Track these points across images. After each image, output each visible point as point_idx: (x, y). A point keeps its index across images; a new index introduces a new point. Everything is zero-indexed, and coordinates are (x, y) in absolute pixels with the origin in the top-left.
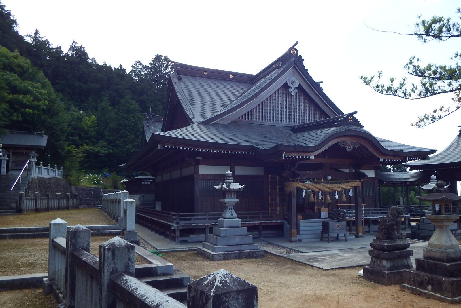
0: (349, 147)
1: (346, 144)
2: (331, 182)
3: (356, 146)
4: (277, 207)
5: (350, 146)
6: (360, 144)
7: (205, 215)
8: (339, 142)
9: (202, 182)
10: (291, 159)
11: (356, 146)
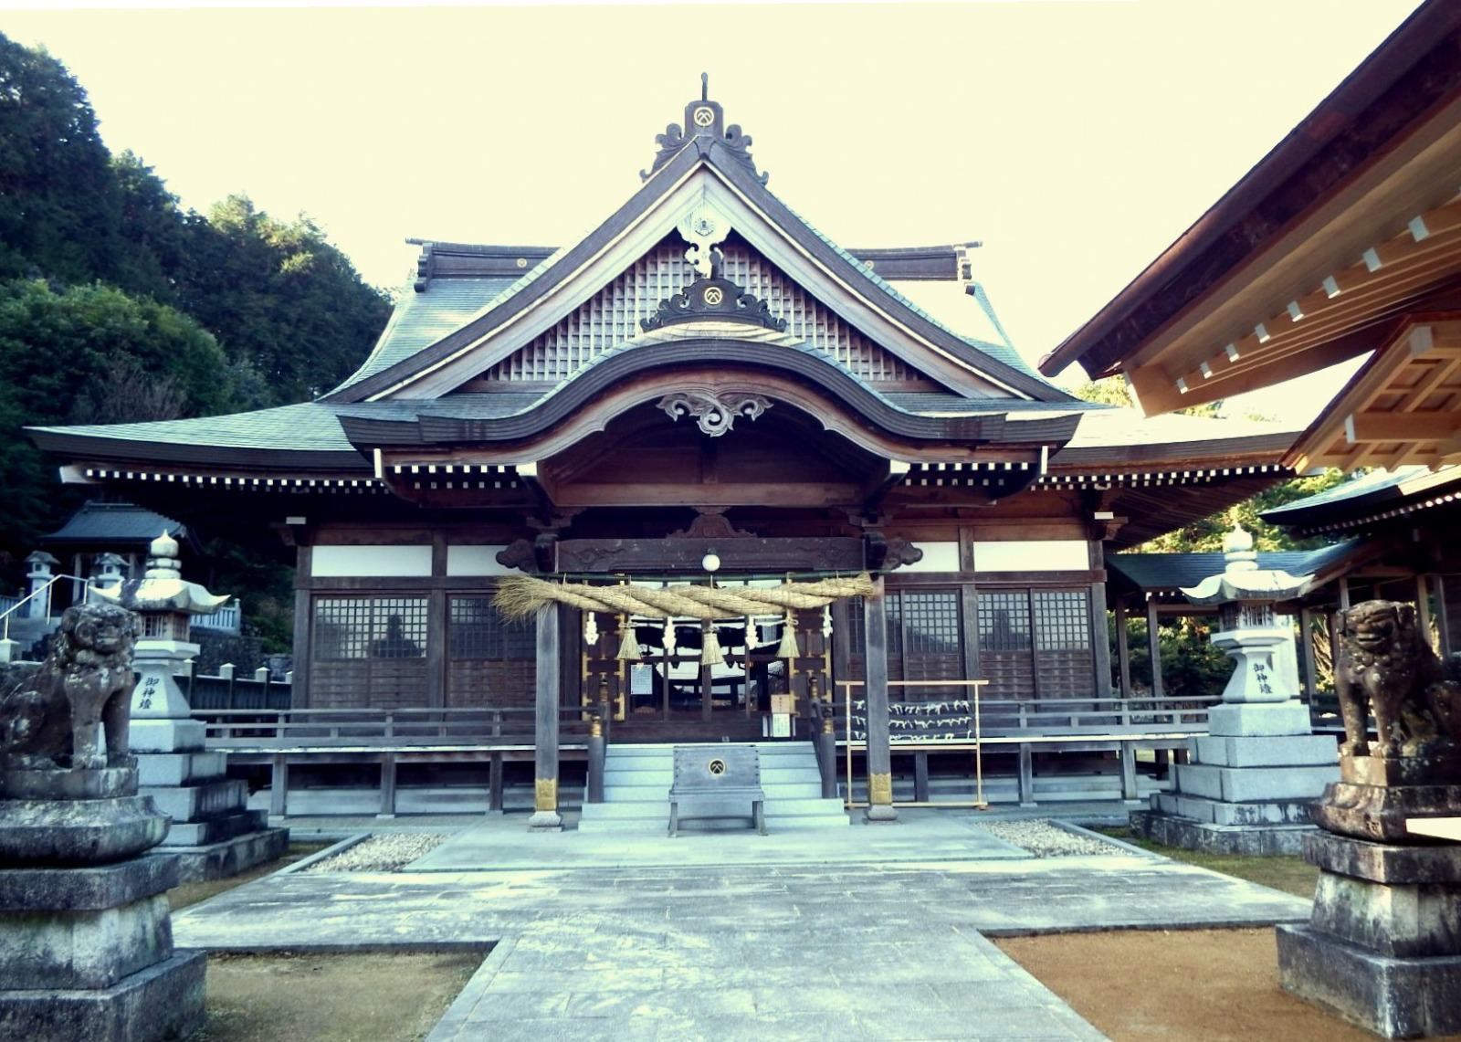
0: (715, 418)
1: (695, 402)
3: (748, 411)
4: (618, 696)
5: (716, 411)
6: (770, 400)
8: (658, 400)
9: (907, 607)
10: (374, 491)
11: (748, 411)
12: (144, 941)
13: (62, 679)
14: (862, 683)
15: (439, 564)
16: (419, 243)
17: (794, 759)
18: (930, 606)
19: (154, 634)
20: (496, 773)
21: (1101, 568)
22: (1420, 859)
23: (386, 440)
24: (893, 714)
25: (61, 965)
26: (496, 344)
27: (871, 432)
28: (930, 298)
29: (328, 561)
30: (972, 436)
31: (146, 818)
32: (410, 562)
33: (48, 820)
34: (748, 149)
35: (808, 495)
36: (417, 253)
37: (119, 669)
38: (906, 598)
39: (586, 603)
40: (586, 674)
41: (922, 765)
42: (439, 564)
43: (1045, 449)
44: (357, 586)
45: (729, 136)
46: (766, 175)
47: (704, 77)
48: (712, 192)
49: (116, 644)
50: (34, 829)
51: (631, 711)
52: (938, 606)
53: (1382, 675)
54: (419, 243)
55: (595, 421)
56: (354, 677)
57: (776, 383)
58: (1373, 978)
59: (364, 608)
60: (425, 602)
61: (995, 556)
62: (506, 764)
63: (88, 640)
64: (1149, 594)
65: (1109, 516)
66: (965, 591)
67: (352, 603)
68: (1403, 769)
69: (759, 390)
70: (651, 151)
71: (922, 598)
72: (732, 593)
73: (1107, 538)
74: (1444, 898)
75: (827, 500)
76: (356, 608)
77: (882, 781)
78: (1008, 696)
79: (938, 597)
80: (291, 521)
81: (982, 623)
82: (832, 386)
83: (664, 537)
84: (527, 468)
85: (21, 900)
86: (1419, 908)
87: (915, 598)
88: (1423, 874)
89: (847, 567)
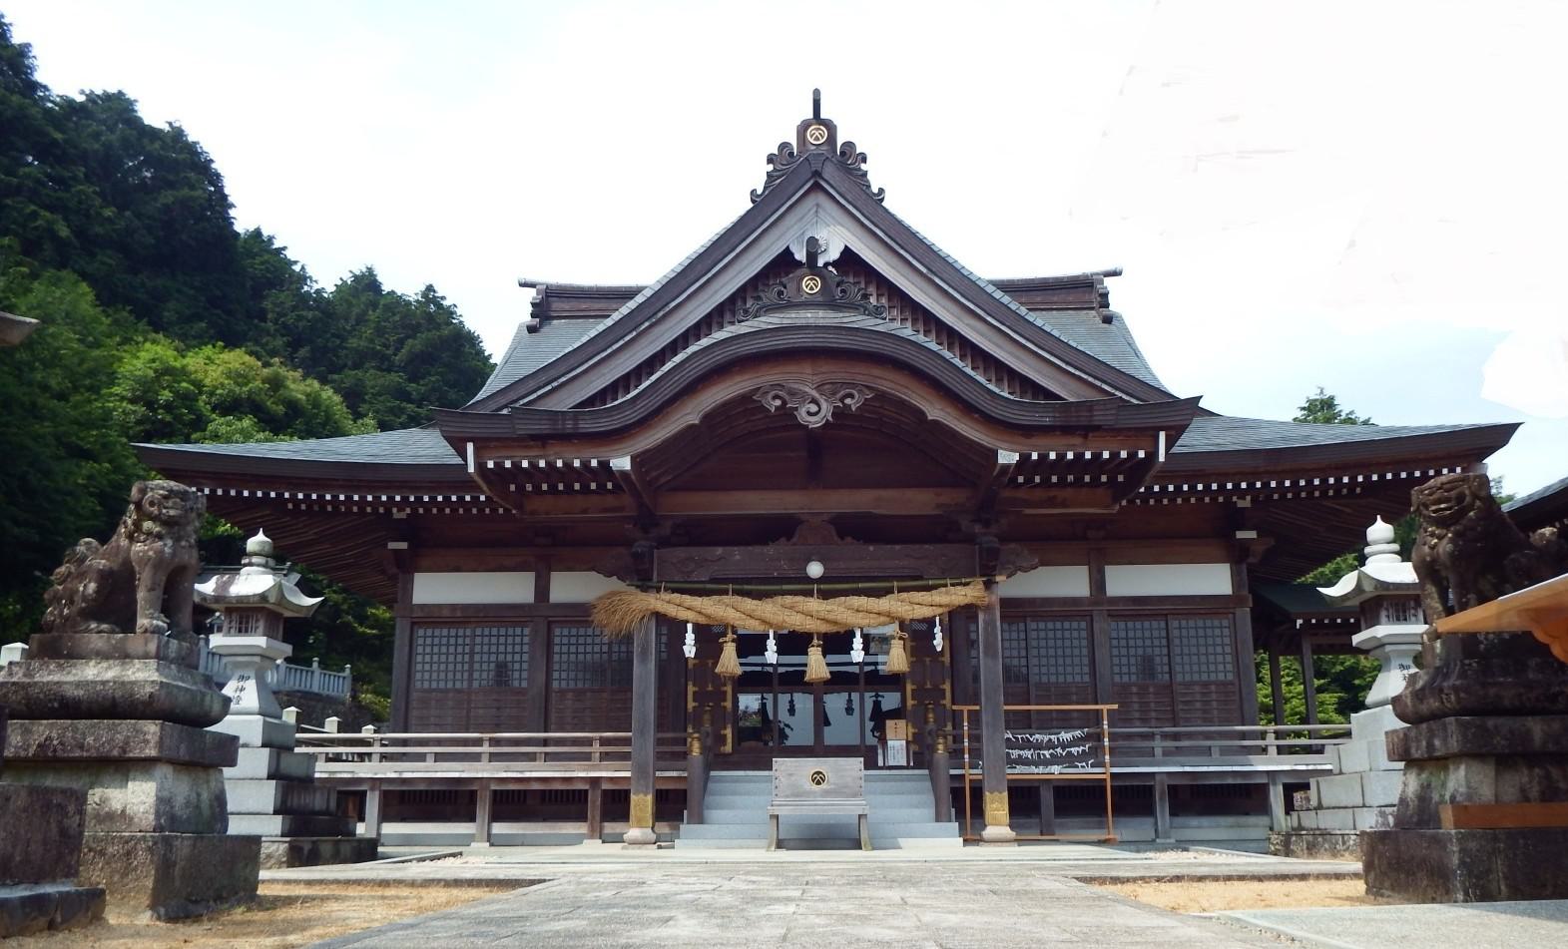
1: (792, 393)
2: (827, 589)
3: (848, 401)
4: (725, 728)
5: (814, 401)
7: (478, 742)
11: (848, 401)
12: (198, 807)
13: (129, 549)
14: (977, 708)
15: (542, 590)
16: (533, 286)
17: (909, 785)
18: (1059, 634)
19: (246, 631)
20: (595, 802)
21: (1245, 592)
22: (1496, 727)
23: (477, 432)
24: (1010, 744)
25: (116, 811)
26: (603, 369)
27: (977, 421)
28: (1069, 327)
29: (432, 589)
30: (1084, 422)
31: (204, 690)
32: (511, 588)
33: (110, 675)
34: (863, 166)
35: (919, 501)
36: (531, 294)
37: (183, 543)
38: (1033, 625)
39: (683, 614)
40: (691, 704)
41: (1047, 798)
42: (542, 590)
43: (1162, 436)
44: (459, 614)
45: (843, 153)
46: (881, 191)
47: (817, 94)
48: (824, 210)
49: (180, 516)
50: (96, 682)
51: (739, 744)
52: (1067, 634)
53: (1456, 545)
54: (533, 286)
55: (690, 414)
56: (453, 708)
57: (877, 371)
58: (1444, 848)
59: (465, 636)
60: (527, 631)
61: (1128, 581)
62: (605, 792)
63: (154, 510)
64: (1299, 622)
65: (1252, 535)
66: (1096, 618)
67: (453, 632)
68: (1482, 643)
69: (860, 379)
70: (765, 178)
71: (1050, 625)
72: (845, 611)
73: (1251, 560)
74: (1526, 772)
75: (938, 506)
76: (457, 636)
77: (997, 806)
78: (1144, 721)
79: (1067, 625)
80: (392, 545)
81: (1116, 661)
82: (935, 371)
83: (766, 543)
84: (622, 463)
85: (81, 747)
86: (1497, 780)
87: (1042, 625)
88: (1500, 743)
89: (958, 574)
